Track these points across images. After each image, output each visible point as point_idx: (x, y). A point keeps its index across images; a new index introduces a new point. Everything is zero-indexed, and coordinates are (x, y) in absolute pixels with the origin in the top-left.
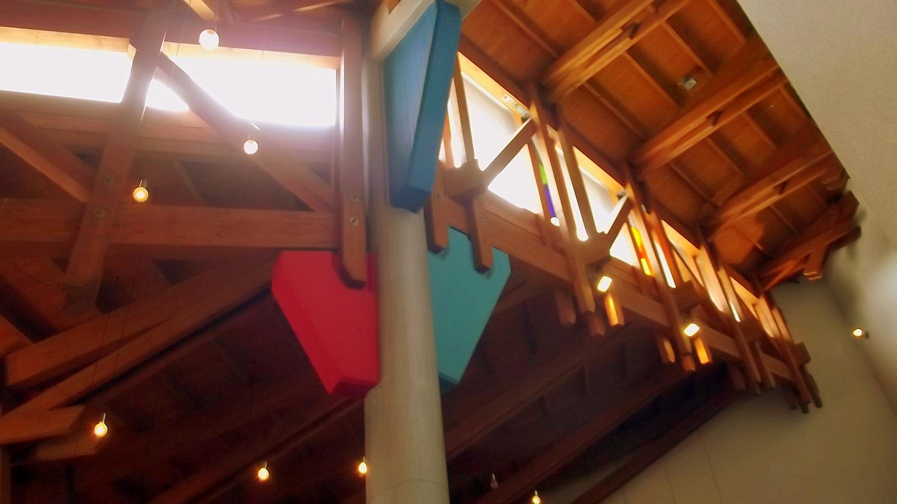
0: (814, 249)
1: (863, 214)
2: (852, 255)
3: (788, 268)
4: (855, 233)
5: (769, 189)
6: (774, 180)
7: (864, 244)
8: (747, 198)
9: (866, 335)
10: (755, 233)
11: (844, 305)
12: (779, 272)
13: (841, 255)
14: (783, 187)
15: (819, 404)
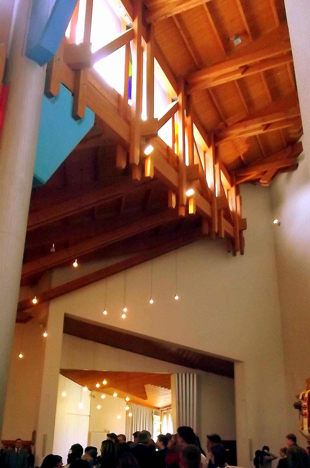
0: (271, 168)
1: (303, 157)
2: (288, 179)
3: (253, 175)
4: (295, 166)
5: (259, 125)
6: (264, 120)
7: (296, 174)
8: (246, 126)
9: (279, 224)
10: (243, 149)
11: (274, 204)
12: (247, 176)
13: (283, 176)
14: (267, 126)
15: (242, 253)
